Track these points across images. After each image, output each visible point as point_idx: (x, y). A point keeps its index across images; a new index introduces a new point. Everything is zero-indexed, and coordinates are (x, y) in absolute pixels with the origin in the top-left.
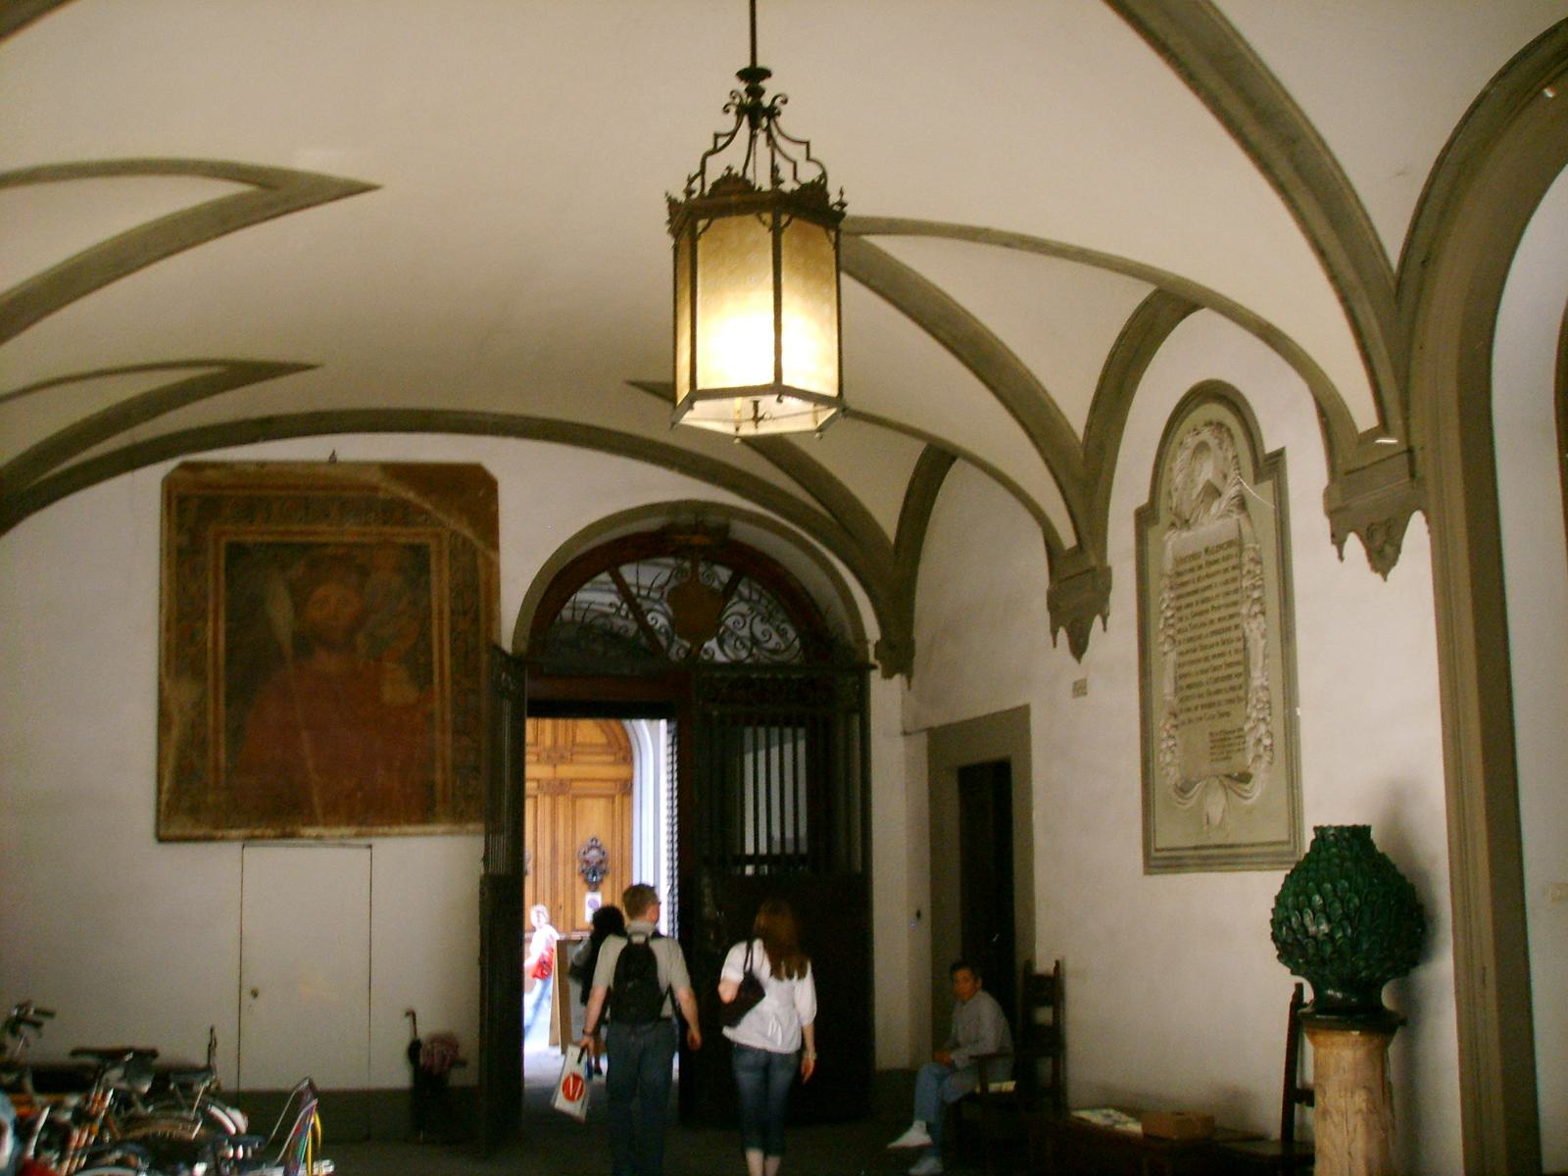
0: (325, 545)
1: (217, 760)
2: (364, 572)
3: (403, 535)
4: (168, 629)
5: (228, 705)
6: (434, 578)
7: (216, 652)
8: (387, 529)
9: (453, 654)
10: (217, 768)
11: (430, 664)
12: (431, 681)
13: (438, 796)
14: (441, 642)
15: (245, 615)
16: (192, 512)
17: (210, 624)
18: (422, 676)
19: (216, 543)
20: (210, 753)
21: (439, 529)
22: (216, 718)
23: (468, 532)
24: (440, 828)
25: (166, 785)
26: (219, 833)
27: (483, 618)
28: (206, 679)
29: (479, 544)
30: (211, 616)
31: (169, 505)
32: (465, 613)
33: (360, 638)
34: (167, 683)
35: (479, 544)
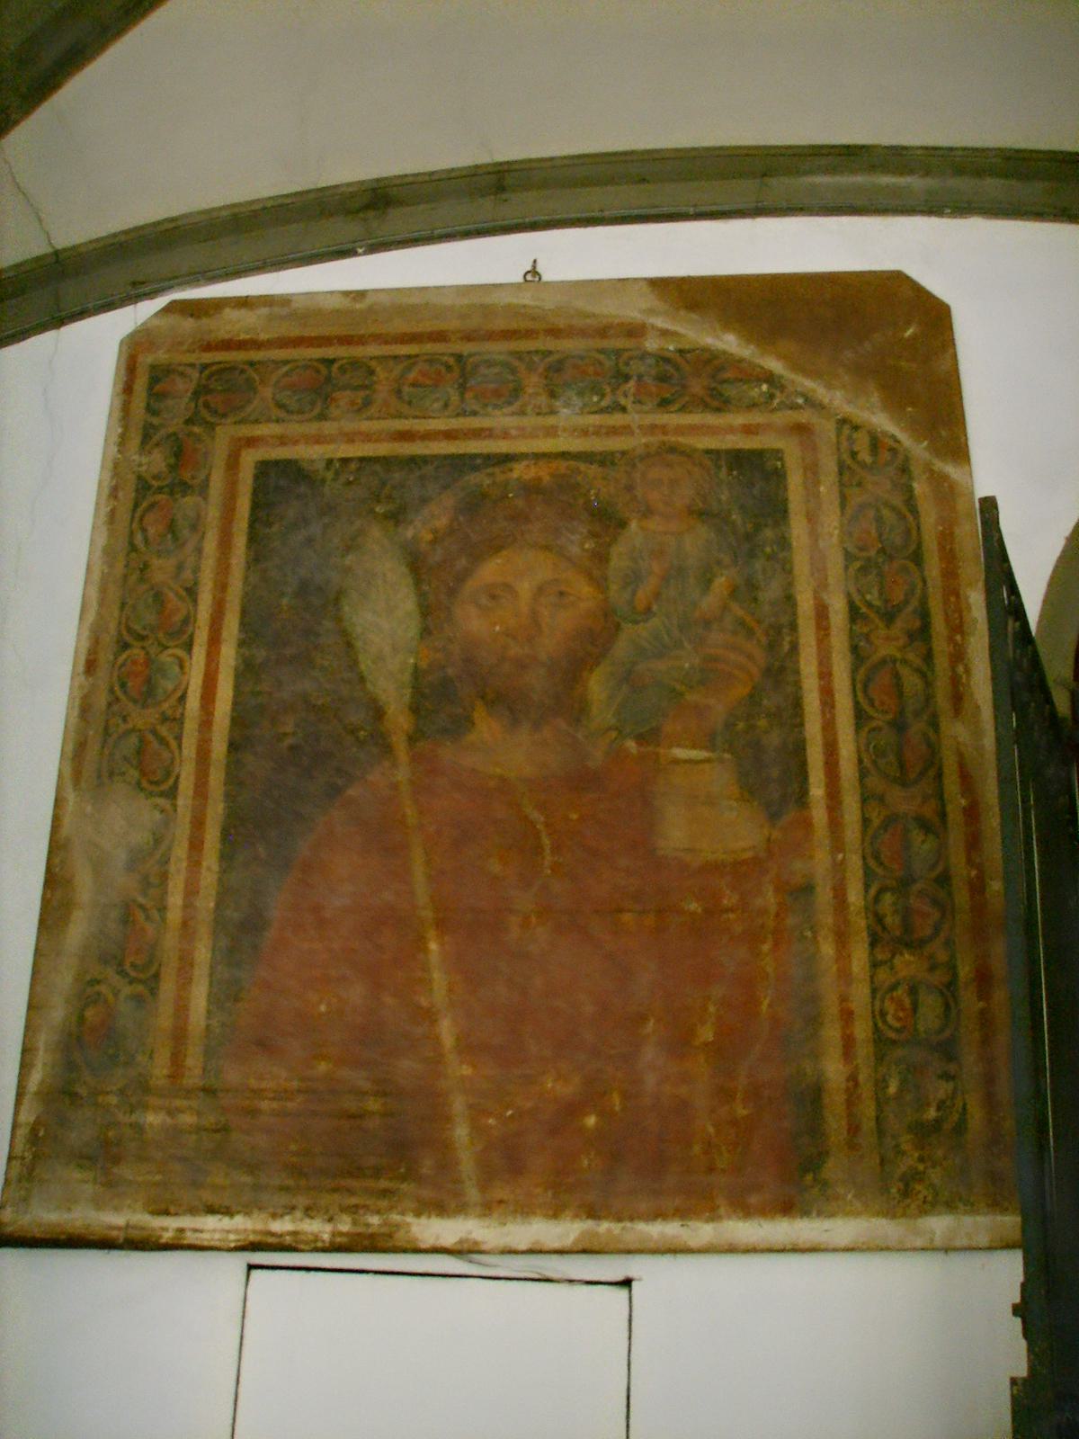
0: (507, 459)
1: (182, 1008)
2: (607, 521)
3: (725, 431)
4: (91, 666)
5: (226, 858)
6: (798, 529)
7: (206, 723)
8: (672, 419)
9: (860, 716)
10: (179, 1036)
11: (800, 749)
12: (804, 792)
13: (835, 1124)
14: (827, 693)
15: (295, 625)
16: (174, 406)
17: (199, 653)
18: (774, 778)
19: (233, 464)
20: (168, 987)
21: (804, 417)
22: (191, 891)
23: (882, 421)
24: (842, 1229)
25: (36, 1077)
26: (167, 1226)
27: (939, 625)
28: (172, 793)
29: (918, 449)
30: (202, 637)
31: (128, 389)
32: (889, 617)
33: (597, 686)
34: (71, 796)
35: (918, 449)
